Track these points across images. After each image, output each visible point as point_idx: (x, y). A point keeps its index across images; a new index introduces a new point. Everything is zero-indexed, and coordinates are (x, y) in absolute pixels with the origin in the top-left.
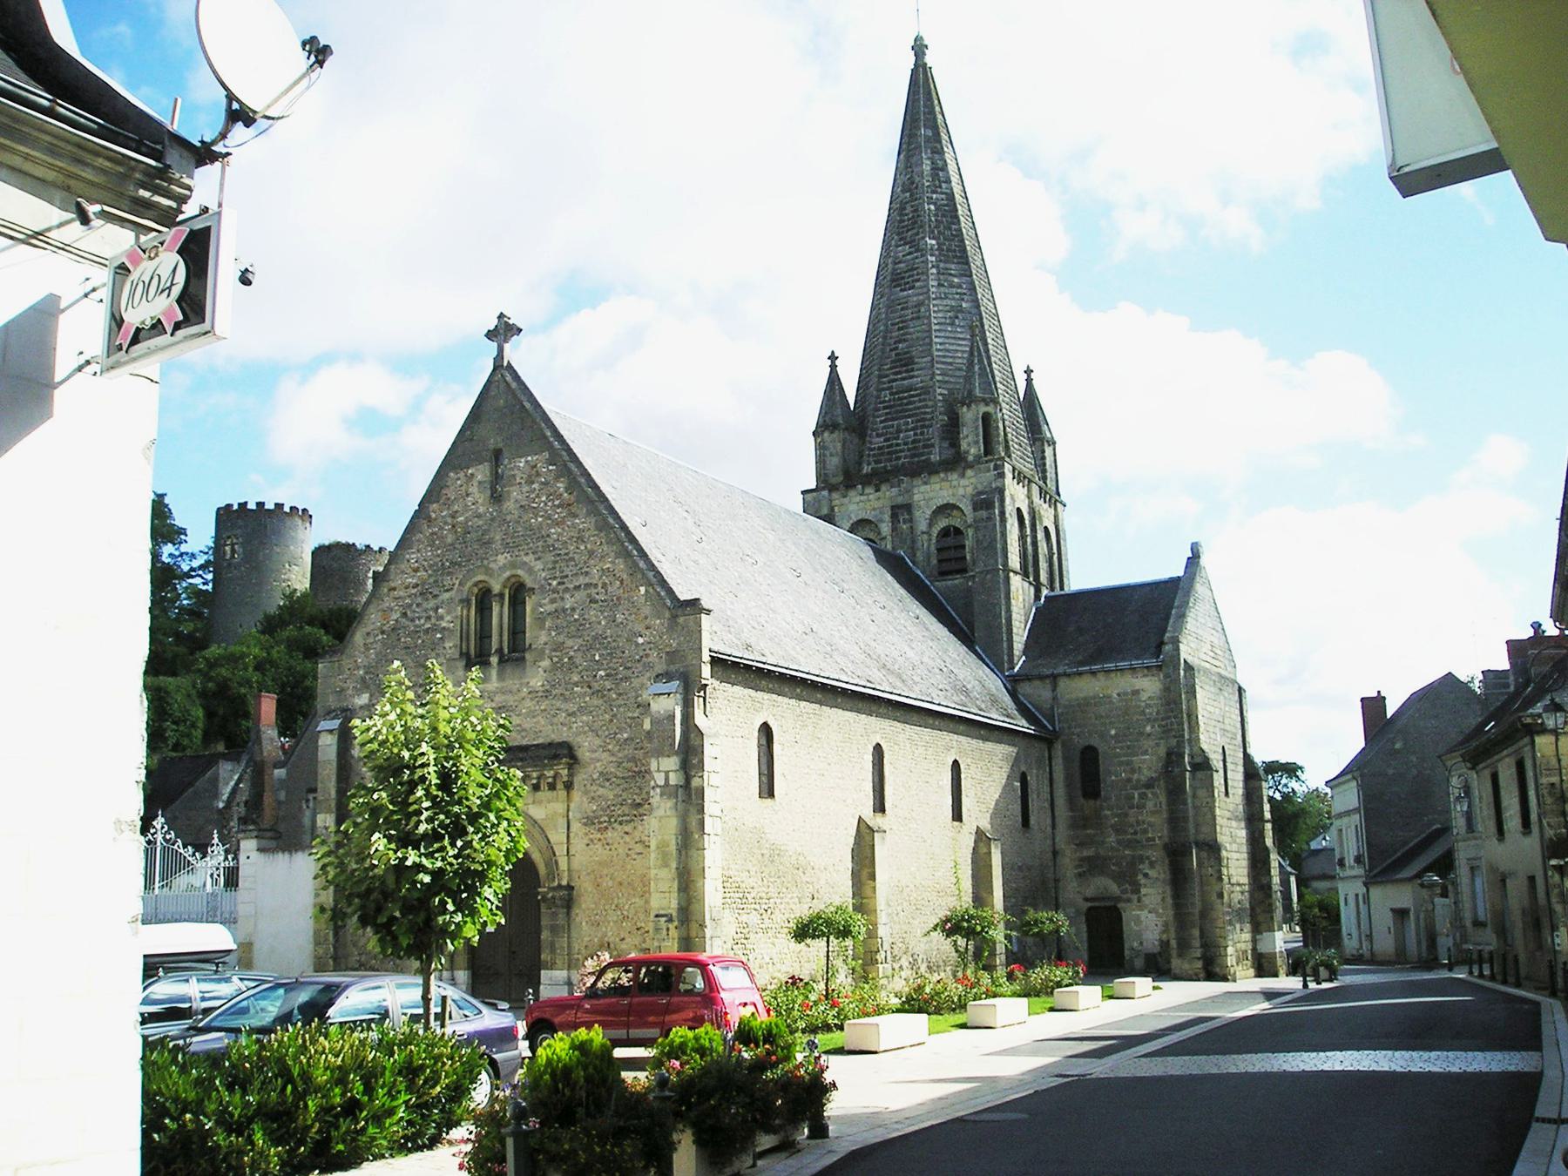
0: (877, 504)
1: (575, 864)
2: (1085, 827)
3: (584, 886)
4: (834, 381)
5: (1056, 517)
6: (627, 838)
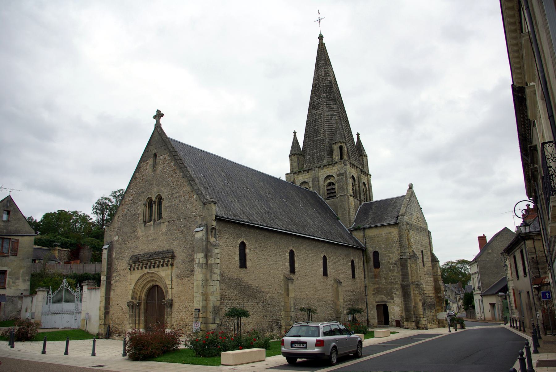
0: (308, 177)
1: (174, 292)
2: (375, 278)
3: (175, 299)
4: (295, 141)
5: (368, 179)
6: (189, 282)
